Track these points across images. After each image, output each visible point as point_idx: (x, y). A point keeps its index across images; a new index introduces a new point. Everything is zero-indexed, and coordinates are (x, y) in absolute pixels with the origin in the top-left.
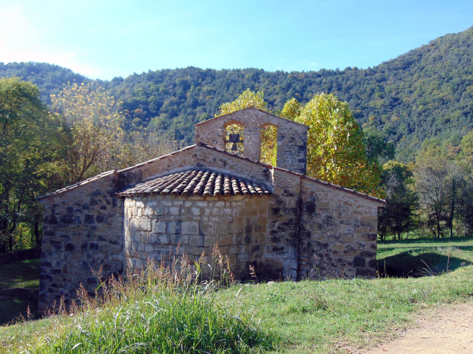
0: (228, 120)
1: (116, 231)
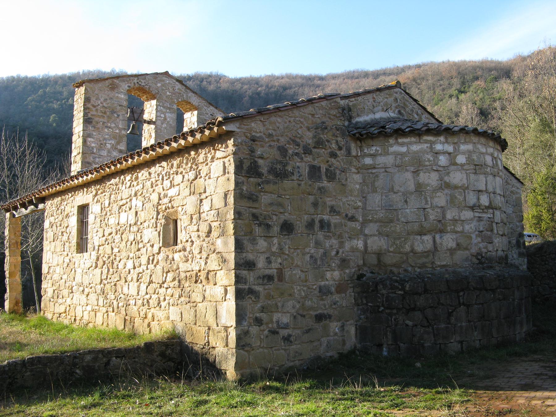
0: (134, 83)
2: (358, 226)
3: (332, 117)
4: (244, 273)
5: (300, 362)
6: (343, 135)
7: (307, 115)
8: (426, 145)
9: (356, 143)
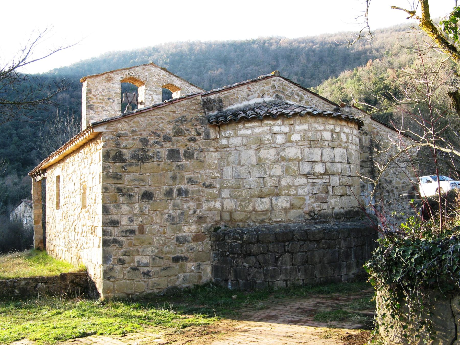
0: (126, 75)
1: (211, 171)
2: (215, 191)
3: (192, 111)
4: (110, 229)
5: (159, 290)
6: (202, 123)
7: (168, 113)
9: (215, 129)
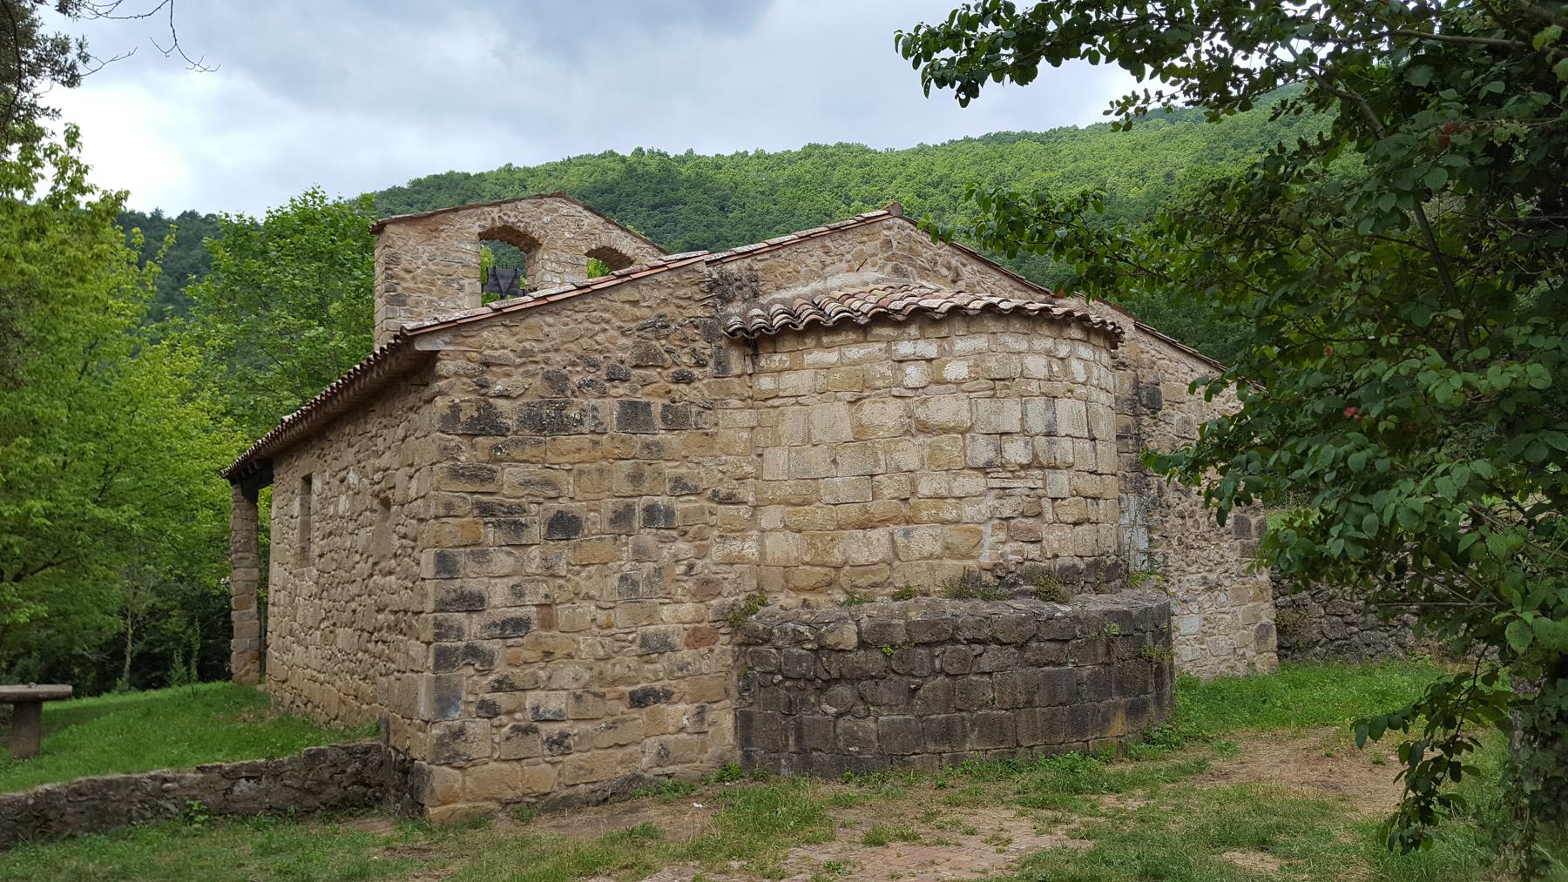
8: (877, 346)
